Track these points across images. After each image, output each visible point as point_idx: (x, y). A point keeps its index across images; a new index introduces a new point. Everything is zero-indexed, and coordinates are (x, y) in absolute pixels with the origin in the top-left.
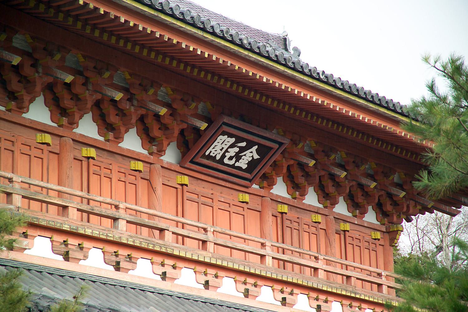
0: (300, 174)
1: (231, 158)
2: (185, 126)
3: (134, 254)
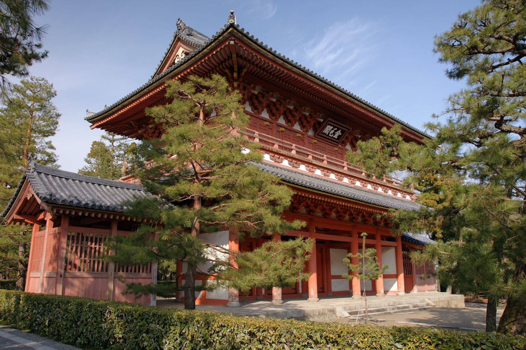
2: (315, 121)
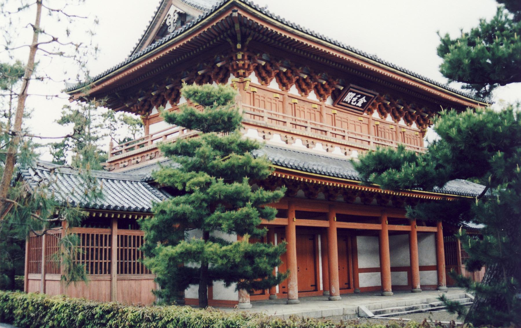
0: (384, 108)
1: (354, 102)
3: (315, 141)
